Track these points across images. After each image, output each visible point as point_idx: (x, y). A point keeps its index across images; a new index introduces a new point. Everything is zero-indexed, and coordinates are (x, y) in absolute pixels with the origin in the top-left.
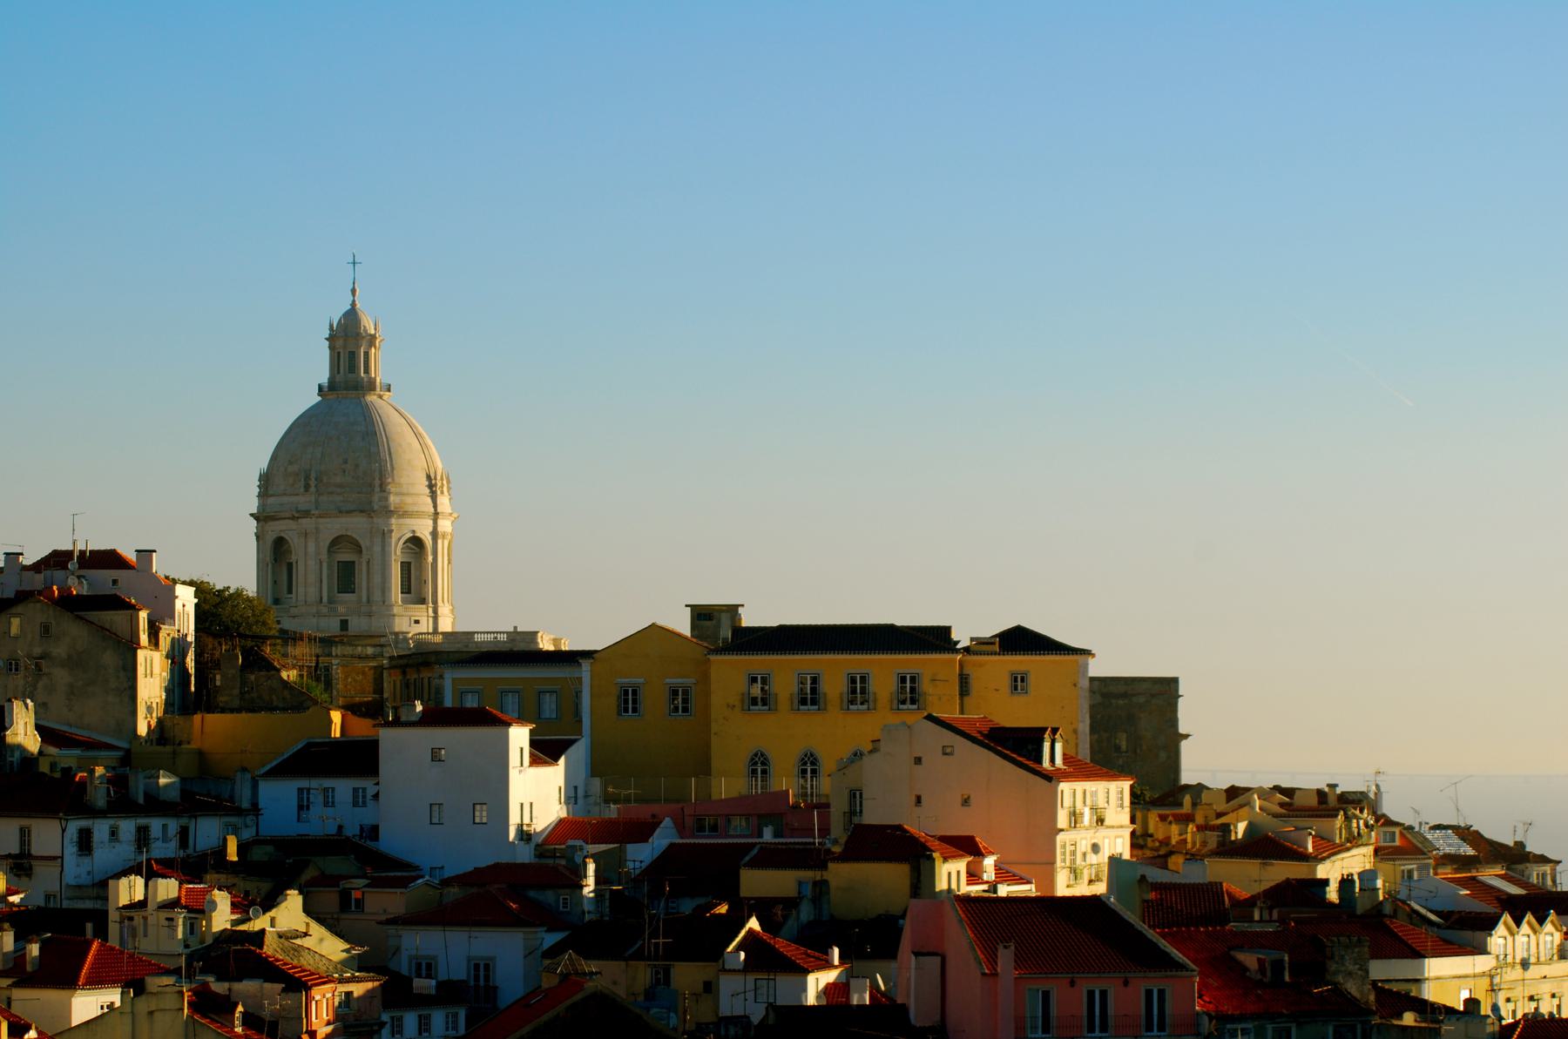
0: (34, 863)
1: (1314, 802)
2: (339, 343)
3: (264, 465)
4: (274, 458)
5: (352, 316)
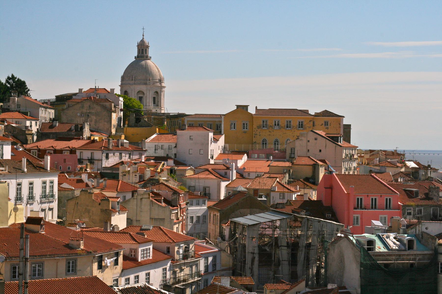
0: (95, 161)
1: (391, 154)
2: (140, 47)
3: (122, 74)
4: (124, 73)
5: (142, 41)
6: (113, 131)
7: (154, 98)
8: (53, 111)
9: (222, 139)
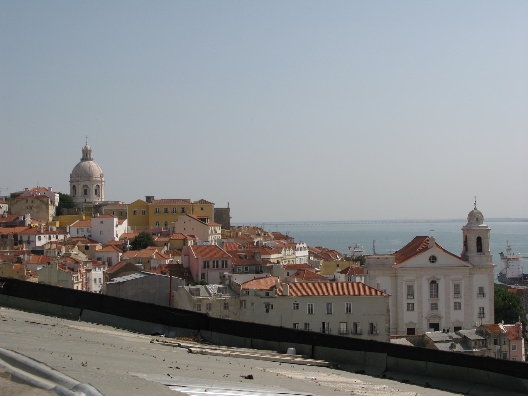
5: (86, 148)
6: (51, 219)
7: (96, 190)
8: (7, 205)
9: (126, 222)
